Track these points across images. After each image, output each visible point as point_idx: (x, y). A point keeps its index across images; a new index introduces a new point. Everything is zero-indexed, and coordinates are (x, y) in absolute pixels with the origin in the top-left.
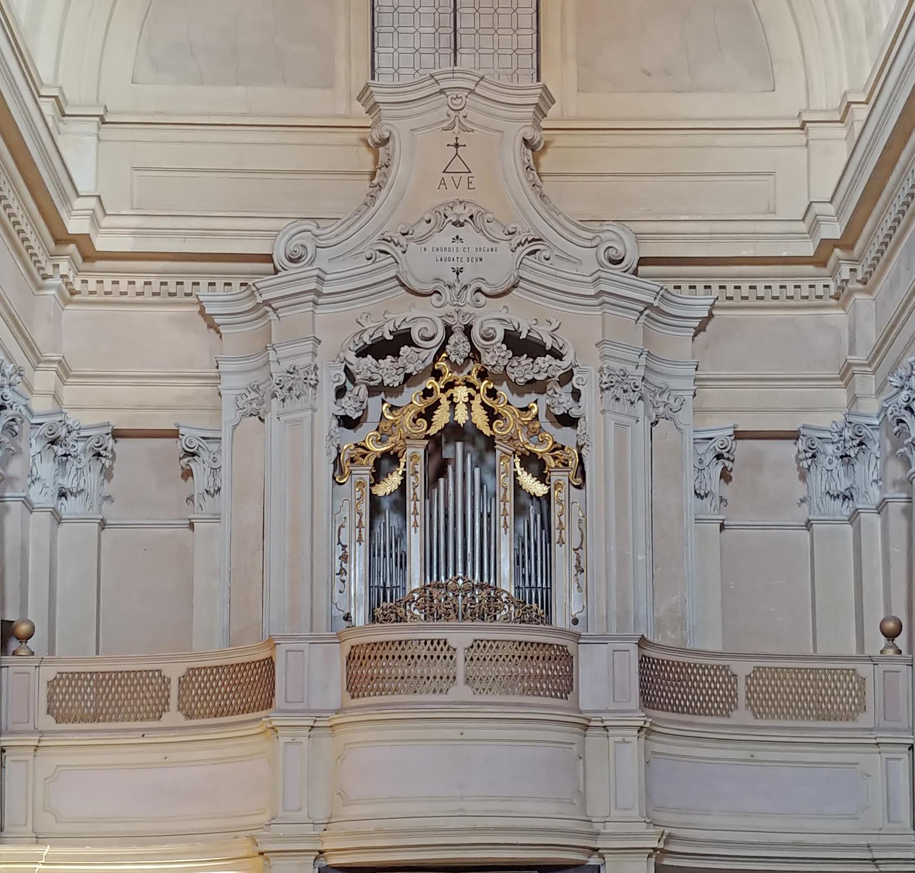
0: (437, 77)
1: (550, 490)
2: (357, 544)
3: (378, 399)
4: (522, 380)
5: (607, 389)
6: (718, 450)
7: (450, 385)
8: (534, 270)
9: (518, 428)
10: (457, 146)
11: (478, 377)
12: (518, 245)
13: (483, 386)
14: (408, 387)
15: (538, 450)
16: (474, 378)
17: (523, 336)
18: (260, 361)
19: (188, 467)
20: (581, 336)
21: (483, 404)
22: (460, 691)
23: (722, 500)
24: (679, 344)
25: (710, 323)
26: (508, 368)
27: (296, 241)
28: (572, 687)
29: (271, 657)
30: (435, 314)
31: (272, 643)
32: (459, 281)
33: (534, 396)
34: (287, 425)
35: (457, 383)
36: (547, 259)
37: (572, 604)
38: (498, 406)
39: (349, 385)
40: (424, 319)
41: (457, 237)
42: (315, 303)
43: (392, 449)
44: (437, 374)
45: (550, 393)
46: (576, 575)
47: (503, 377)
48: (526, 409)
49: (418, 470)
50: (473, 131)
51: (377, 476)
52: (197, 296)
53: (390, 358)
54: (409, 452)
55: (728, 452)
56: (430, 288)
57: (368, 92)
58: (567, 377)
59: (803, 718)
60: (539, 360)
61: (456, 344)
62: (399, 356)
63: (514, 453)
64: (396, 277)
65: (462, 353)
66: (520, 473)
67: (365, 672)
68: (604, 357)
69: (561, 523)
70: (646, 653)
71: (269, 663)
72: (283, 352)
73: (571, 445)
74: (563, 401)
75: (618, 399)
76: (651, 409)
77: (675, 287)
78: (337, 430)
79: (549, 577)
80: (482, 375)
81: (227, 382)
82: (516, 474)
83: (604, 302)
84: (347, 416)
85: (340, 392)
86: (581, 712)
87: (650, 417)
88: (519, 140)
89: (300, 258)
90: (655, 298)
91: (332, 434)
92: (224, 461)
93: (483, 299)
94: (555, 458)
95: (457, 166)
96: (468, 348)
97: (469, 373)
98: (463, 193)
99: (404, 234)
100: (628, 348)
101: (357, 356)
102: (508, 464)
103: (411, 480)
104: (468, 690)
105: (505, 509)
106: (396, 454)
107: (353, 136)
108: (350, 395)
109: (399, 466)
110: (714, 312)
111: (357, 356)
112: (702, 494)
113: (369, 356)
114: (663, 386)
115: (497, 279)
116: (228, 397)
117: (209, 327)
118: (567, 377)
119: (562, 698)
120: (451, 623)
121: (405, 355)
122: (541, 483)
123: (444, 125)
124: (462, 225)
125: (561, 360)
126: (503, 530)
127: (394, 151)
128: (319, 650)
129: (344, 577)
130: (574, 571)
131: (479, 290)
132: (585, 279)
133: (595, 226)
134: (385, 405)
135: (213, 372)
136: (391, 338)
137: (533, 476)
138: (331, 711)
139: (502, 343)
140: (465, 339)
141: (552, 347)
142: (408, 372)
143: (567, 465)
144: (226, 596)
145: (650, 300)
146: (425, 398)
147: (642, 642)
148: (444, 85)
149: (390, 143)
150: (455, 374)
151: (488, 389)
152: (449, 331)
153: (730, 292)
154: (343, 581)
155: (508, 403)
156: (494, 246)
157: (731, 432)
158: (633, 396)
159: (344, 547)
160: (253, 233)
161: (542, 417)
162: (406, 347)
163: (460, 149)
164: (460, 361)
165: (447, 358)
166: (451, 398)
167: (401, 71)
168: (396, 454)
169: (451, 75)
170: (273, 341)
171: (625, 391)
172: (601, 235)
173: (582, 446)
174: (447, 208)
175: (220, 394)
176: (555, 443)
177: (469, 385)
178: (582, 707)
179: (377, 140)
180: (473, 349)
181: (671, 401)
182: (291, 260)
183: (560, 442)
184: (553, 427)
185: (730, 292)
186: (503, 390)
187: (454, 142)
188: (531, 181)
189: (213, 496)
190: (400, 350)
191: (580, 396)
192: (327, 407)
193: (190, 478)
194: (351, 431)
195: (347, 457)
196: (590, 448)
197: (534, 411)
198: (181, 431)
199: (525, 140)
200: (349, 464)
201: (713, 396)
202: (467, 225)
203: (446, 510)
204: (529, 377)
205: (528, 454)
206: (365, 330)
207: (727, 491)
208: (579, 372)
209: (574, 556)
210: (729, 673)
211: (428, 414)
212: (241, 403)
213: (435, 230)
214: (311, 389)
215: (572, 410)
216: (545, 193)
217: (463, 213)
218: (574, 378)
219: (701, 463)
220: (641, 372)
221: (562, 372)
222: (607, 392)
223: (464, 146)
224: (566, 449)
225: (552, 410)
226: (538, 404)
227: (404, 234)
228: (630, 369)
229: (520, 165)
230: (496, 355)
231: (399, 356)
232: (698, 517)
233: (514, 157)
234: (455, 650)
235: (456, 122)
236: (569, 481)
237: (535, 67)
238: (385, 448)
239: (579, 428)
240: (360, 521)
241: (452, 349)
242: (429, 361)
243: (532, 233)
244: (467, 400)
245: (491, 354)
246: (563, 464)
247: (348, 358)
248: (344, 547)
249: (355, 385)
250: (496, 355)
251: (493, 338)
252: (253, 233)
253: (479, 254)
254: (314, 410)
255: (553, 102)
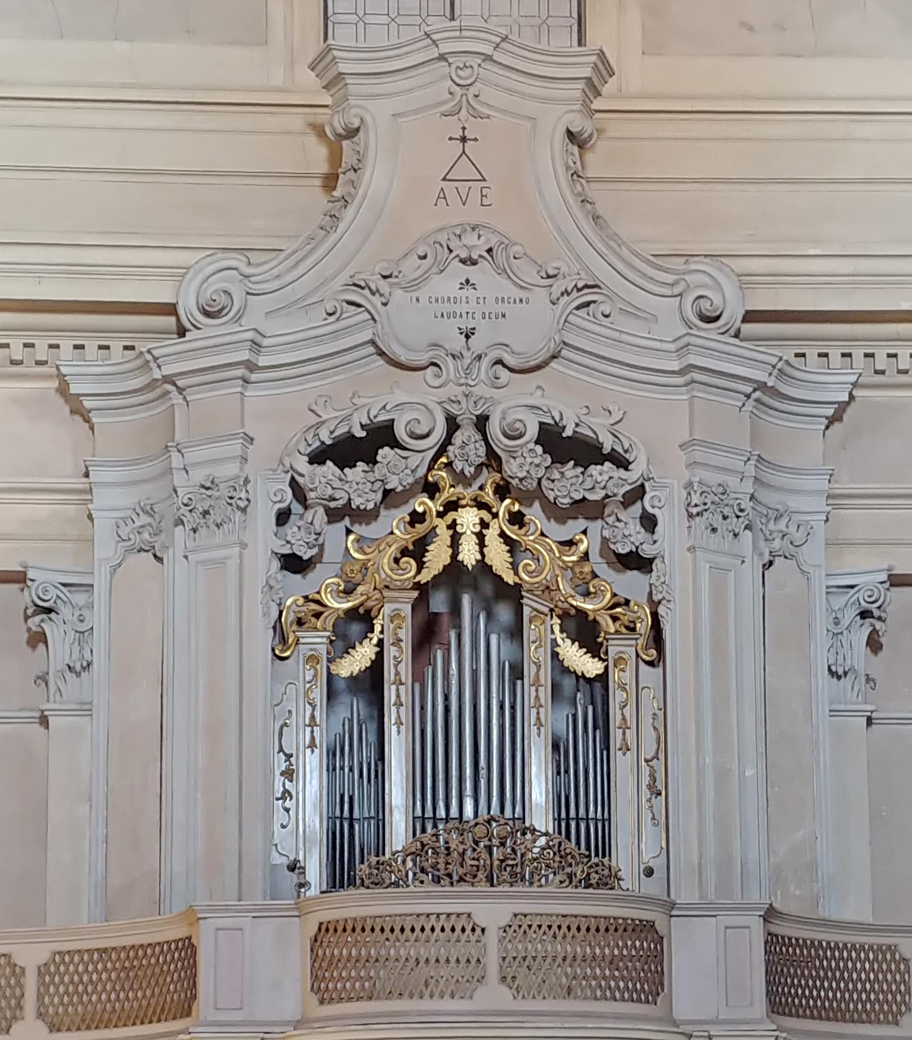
0: (435, 37)
1: (606, 668)
2: (308, 751)
3: (340, 527)
4: (567, 500)
5: (698, 514)
6: (863, 604)
7: (452, 506)
8: (587, 333)
9: (557, 572)
10: (464, 139)
11: (495, 493)
12: (562, 294)
13: (504, 507)
14: (387, 508)
15: (588, 606)
16: (489, 496)
17: (568, 433)
18: (157, 467)
19: (39, 630)
20: (658, 433)
21: (502, 535)
22: (494, 995)
23: (868, 679)
24: (802, 442)
25: (849, 410)
26: (544, 482)
27: (216, 284)
28: (662, 985)
29: (189, 938)
30: (431, 399)
31: (191, 916)
32: (469, 349)
33: (582, 523)
34: (200, 568)
35: (464, 502)
36: (607, 316)
37: (643, 846)
38: (529, 539)
39: (297, 508)
40: (415, 406)
41: (468, 281)
42: (246, 381)
43: (362, 604)
44: (431, 489)
45: (611, 520)
46: (649, 800)
47: (537, 494)
48: (570, 543)
49: (403, 638)
50: (488, 117)
51: (343, 643)
52: (57, 367)
53: (361, 466)
54: (388, 609)
55: (879, 607)
56: (423, 358)
57: (329, 58)
58: (638, 493)
59: (862, 947)
60: (594, 470)
61: (464, 444)
62: (375, 462)
63: (552, 610)
64: (373, 342)
65: (472, 458)
66: (560, 641)
67: (337, 965)
68: (692, 465)
69: (624, 719)
70: (774, 929)
71: (187, 949)
72: (192, 456)
73: (639, 598)
74: (629, 534)
75: (714, 530)
76: (762, 544)
77: (797, 355)
78: (279, 577)
79: (606, 802)
80: (502, 491)
81: (102, 499)
82: (554, 643)
83: (694, 382)
84: (294, 555)
85: (283, 517)
86: (675, 1023)
87: (761, 555)
88: (561, 132)
89: (223, 308)
90: (770, 374)
91: (272, 583)
92: (98, 619)
93: (505, 374)
94: (615, 619)
95: (464, 170)
96: (482, 451)
97: (481, 488)
98: (474, 213)
99: (385, 277)
100: (730, 450)
101: (311, 462)
102: (542, 627)
103: (390, 652)
104: (505, 992)
105: (537, 697)
106: (368, 612)
107: (296, 120)
108: (300, 523)
109: (372, 632)
110: (855, 393)
111: (311, 462)
112: (841, 672)
113: (329, 463)
114: (779, 507)
115: (528, 343)
116: (104, 524)
117: (72, 412)
118: (638, 493)
119: (648, 1002)
120: (479, 889)
121: (385, 461)
122: (593, 657)
123: (445, 108)
124: (474, 263)
125: (626, 469)
126: (534, 729)
127: (366, 149)
128: (267, 928)
129: (288, 804)
130: (645, 793)
131: (499, 362)
132: (665, 346)
133: (677, 264)
134: (352, 537)
135: (80, 483)
136: (364, 434)
137: (581, 647)
138: (287, 1023)
139: (536, 443)
140: (478, 437)
141: (613, 449)
142: (388, 487)
143: (633, 630)
144: (101, 831)
145: (761, 376)
146: (413, 526)
147: (770, 914)
148: (444, 48)
149: (361, 133)
150: (460, 489)
151: (510, 513)
152: (453, 425)
153: (881, 362)
154: (287, 810)
155: (542, 534)
156: (523, 294)
157: (884, 577)
158: (738, 525)
159: (289, 757)
160: (143, 272)
161: (595, 556)
162: (387, 449)
163: (469, 144)
164: (469, 471)
165: (449, 465)
166: (453, 525)
167: (369, 19)
168: (368, 612)
169: (457, 34)
170: (177, 438)
171: (725, 518)
172: (686, 277)
173: (659, 602)
174: (452, 236)
175: (90, 517)
176: (614, 595)
177: (481, 505)
178: (677, 1015)
179: (341, 131)
180: (491, 453)
181: (792, 529)
182: (207, 314)
183: (623, 594)
184: (611, 572)
185: (881, 362)
186: (534, 514)
187: (458, 134)
188: (579, 194)
189: (78, 675)
190: (376, 454)
191: (655, 525)
192: (264, 541)
193: (41, 646)
194: (298, 577)
195: (292, 617)
196: (671, 606)
197: (583, 547)
198: (31, 574)
199: (570, 134)
200: (295, 627)
201: (856, 520)
202: (483, 264)
203: (447, 698)
204: (578, 497)
205: (573, 612)
206: (323, 423)
207: (877, 665)
208: (654, 488)
209: (645, 769)
210: (897, 956)
211: (417, 551)
212: (124, 532)
213: (435, 270)
214: (239, 513)
215: (644, 546)
216: (600, 212)
217: (476, 244)
218: (647, 498)
219: (837, 624)
220: (748, 487)
221: (628, 488)
222: (698, 519)
223: (476, 140)
224: (632, 604)
225: (612, 546)
226: (590, 538)
227: (385, 277)
228: (732, 482)
229: (561, 169)
230: (525, 462)
231: (375, 462)
232: (834, 707)
233: (551, 153)
234: (483, 930)
235: (463, 103)
236: (638, 655)
237: (575, 15)
238: (350, 604)
239: (654, 574)
240: (313, 717)
241: (457, 451)
242: (422, 472)
243: (583, 275)
244: (478, 529)
245: (519, 460)
246: (627, 628)
247: (296, 466)
248: (289, 757)
249: (306, 508)
250: (525, 462)
251: (521, 436)
252: (143, 272)
253: (500, 308)
254: (243, 546)
255: (611, 74)
